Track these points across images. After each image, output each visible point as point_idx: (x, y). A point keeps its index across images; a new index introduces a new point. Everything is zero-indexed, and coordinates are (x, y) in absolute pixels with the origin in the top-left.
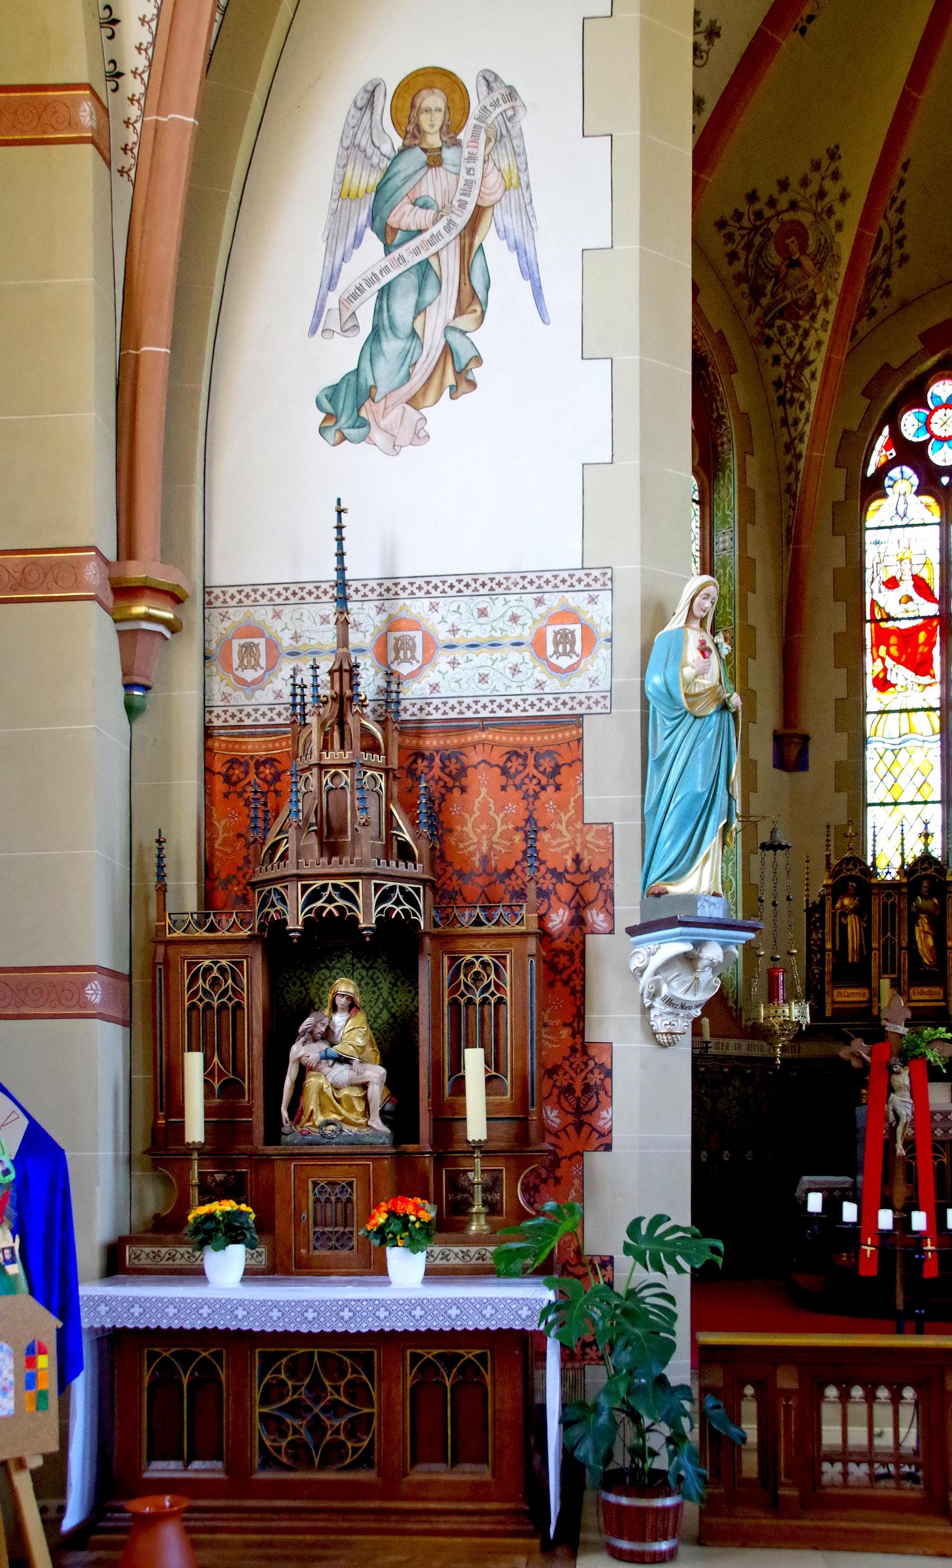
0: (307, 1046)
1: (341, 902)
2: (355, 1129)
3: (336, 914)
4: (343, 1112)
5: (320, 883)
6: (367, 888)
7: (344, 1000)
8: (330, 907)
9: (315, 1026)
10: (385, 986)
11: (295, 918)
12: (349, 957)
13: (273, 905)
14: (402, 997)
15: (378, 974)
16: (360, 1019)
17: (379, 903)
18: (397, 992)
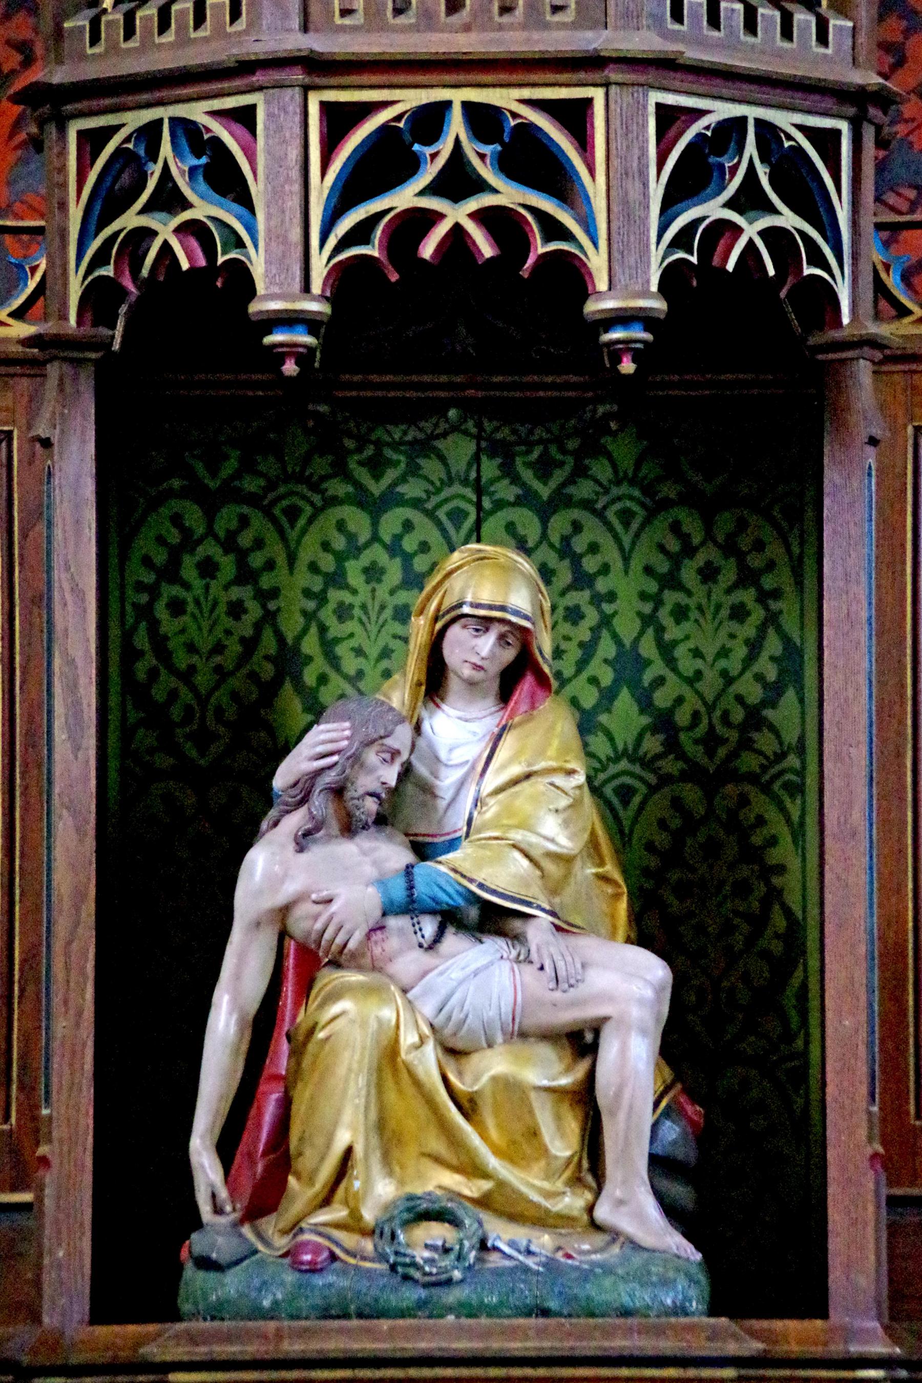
0: (317, 853)
1: (509, 194)
2: (544, 1241)
3: (487, 249)
4: (493, 1162)
5: (412, 99)
6: (624, 128)
7: (487, 643)
8: (458, 214)
9: (356, 759)
10: (626, 587)
11: (287, 262)
12: (460, 450)
13: (169, 199)
14: (709, 648)
15: (593, 531)
16: (548, 732)
17: (674, 198)
18: (680, 614)
